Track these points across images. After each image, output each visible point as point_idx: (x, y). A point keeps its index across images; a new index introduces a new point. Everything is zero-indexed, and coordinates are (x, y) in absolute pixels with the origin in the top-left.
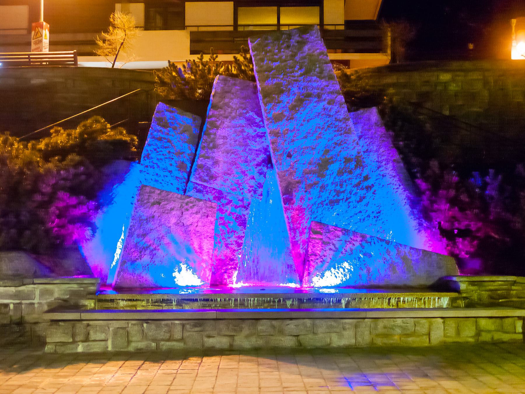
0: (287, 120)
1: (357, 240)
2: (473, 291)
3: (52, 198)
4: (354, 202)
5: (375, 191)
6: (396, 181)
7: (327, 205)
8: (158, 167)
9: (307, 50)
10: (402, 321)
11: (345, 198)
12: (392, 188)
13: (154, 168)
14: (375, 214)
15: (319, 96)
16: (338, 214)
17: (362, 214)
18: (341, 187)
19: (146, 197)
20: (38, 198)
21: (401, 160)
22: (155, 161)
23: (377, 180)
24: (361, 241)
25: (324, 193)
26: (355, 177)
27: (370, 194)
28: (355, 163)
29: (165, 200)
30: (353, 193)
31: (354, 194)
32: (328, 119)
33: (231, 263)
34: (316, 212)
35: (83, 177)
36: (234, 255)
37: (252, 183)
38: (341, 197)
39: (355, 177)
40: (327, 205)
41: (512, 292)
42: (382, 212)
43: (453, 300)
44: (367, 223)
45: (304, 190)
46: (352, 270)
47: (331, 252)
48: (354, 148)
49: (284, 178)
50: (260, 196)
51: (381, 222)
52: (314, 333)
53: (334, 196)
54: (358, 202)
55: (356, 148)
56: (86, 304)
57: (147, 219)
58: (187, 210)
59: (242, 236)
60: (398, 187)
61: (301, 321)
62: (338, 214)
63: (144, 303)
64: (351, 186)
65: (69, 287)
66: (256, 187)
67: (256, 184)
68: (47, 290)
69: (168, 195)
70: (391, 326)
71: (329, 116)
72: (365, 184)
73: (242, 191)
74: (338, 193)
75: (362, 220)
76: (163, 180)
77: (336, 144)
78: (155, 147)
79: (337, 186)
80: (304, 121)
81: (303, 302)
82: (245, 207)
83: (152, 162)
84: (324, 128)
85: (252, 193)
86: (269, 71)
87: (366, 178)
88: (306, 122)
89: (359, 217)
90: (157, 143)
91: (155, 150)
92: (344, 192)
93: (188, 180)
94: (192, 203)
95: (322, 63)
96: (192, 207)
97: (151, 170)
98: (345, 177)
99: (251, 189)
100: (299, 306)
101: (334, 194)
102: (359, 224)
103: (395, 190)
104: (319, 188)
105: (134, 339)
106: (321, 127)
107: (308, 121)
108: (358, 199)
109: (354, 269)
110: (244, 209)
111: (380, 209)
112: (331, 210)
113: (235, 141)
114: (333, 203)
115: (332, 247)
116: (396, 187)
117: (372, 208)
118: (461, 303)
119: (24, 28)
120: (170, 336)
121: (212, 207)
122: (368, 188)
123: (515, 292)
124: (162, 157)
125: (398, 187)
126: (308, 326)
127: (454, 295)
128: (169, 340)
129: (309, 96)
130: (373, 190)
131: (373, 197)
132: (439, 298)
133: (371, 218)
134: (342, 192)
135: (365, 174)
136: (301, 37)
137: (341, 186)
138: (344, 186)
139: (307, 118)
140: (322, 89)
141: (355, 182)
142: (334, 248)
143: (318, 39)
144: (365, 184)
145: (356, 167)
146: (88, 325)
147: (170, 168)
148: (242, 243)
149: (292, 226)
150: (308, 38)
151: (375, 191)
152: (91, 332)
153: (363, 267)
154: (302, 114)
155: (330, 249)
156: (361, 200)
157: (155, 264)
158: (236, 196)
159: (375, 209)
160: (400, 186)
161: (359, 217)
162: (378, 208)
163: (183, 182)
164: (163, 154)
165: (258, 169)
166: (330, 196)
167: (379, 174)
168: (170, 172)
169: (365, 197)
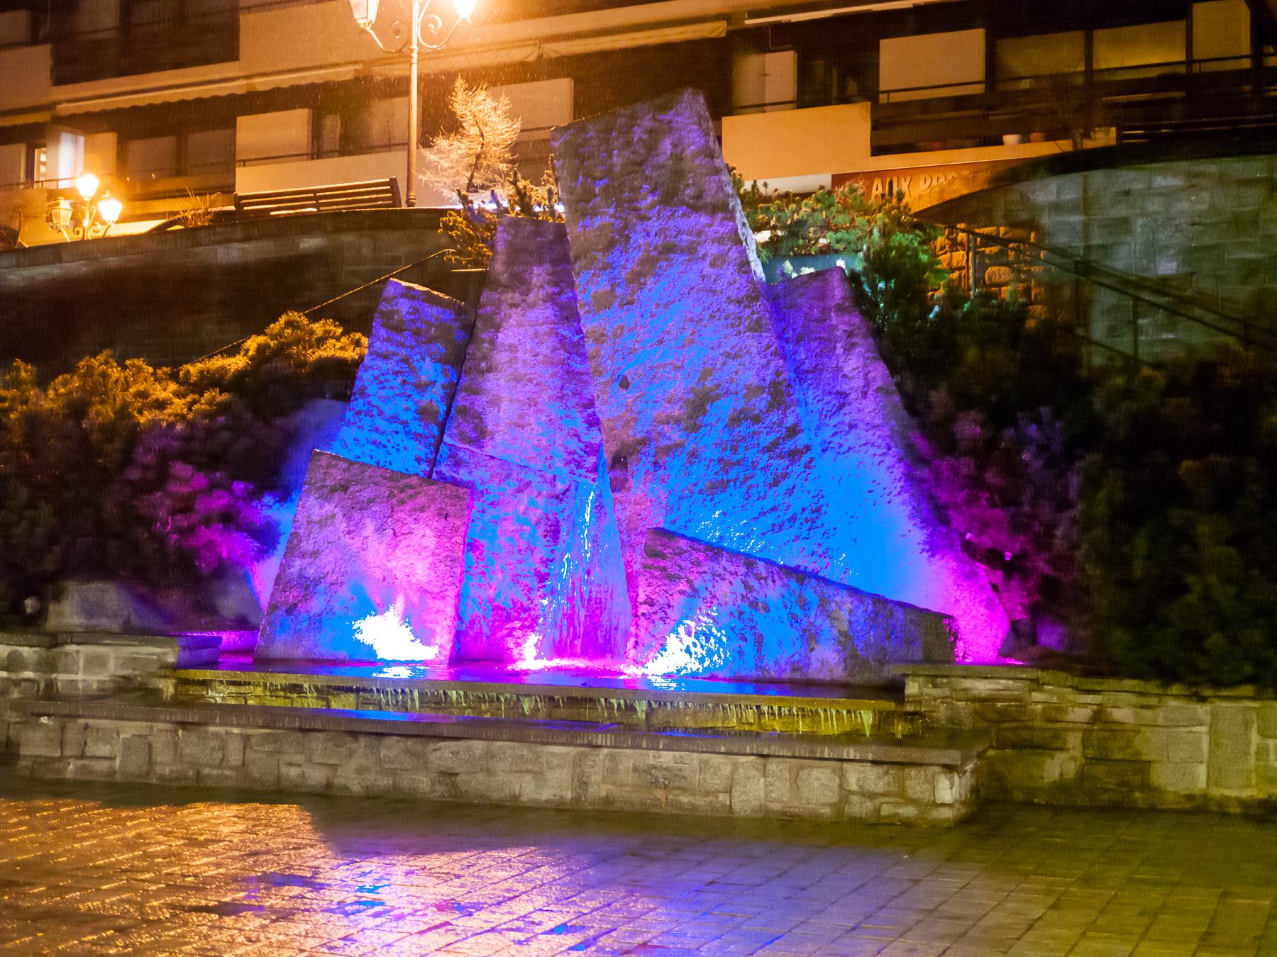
0: (621, 306)
1: (736, 573)
2: (935, 699)
3: (162, 478)
4: (761, 484)
5: (812, 460)
6: (879, 437)
7: (701, 492)
8: (381, 413)
9: (669, 147)
10: (674, 757)
11: (742, 477)
12: (869, 452)
13: (372, 416)
14: (806, 514)
15: (691, 250)
16: (724, 514)
17: (778, 513)
18: (735, 453)
19: (320, 476)
20: (134, 474)
21: (894, 388)
22: (375, 401)
23: (835, 434)
24: (746, 575)
25: (695, 467)
26: (765, 430)
27: (798, 468)
28: (769, 398)
29: (357, 482)
30: (759, 467)
31: (762, 469)
32: (710, 300)
33: (523, 615)
34: (675, 508)
35: (226, 435)
36: (529, 599)
37: (574, 445)
38: (733, 474)
39: (765, 430)
40: (701, 492)
41: (1033, 706)
42: (824, 509)
43: (884, 719)
44: (788, 533)
45: (652, 459)
46: (724, 639)
47: (683, 598)
48: (769, 363)
49: (613, 433)
50: (590, 472)
51: (821, 531)
52: (489, 772)
53: (717, 473)
54: (771, 486)
55: (773, 365)
56: (161, 686)
57: (320, 521)
58: (403, 502)
59: (548, 560)
60: (885, 450)
61: (463, 744)
62: (724, 514)
63: (259, 691)
64: (756, 450)
65: (132, 653)
66: (581, 453)
67: (582, 445)
68: (97, 657)
69: (363, 472)
70: (646, 768)
71: (714, 292)
72: (790, 445)
73: (549, 462)
74: (726, 465)
75: (776, 528)
76: (389, 441)
77: (727, 355)
78: (376, 373)
79: (725, 449)
80: (658, 305)
81: (558, 706)
82: (557, 497)
83: (369, 403)
84: (702, 320)
85: (573, 466)
86: (585, 201)
87: (793, 431)
88: (661, 309)
89: (769, 520)
90: (380, 363)
91: (376, 378)
92: (738, 463)
93: (440, 441)
94: (411, 487)
95: (701, 174)
96: (411, 497)
97: (366, 420)
98: (743, 429)
99: (570, 458)
100: (550, 715)
101: (718, 468)
102: (769, 536)
103: (878, 459)
104: (684, 456)
105: (159, 759)
106: (696, 319)
107: (666, 306)
108: (770, 479)
109: (728, 638)
110: (555, 501)
111: (821, 503)
112: (709, 504)
113: (537, 355)
114: (719, 487)
115: (683, 586)
116: (880, 451)
117: (800, 501)
118: (900, 729)
119: (304, 152)
120: (223, 759)
121: (459, 497)
122: (794, 455)
123: (1039, 707)
124: (390, 393)
125: (885, 450)
126: (477, 756)
127: (890, 705)
128: (219, 766)
129: (669, 250)
130: (805, 458)
131: (804, 475)
132: (849, 712)
133: (798, 523)
134: (734, 464)
135: (790, 420)
136: (657, 120)
137: (735, 450)
138: (741, 450)
139: (665, 300)
140: (699, 234)
141: (766, 440)
142: (689, 590)
143: (691, 121)
144: (790, 445)
145: (771, 407)
146: (87, 726)
147: (404, 417)
148: (548, 574)
149: (626, 538)
150: (671, 122)
151: (812, 460)
152: (90, 743)
153: (748, 636)
154: (654, 289)
155: (682, 593)
156: (776, 483)
157: (334, 614)
158: (538, 473)
159: (807, 501)
160: (889, 449)
161: (769, 520)
162: (816, 500)
163: (431, 445)
164: (391, 388)
165: (585, 414)
166: (709, 472)
167: (842, 423)
168: (405, 424)
169: (787, 473)
